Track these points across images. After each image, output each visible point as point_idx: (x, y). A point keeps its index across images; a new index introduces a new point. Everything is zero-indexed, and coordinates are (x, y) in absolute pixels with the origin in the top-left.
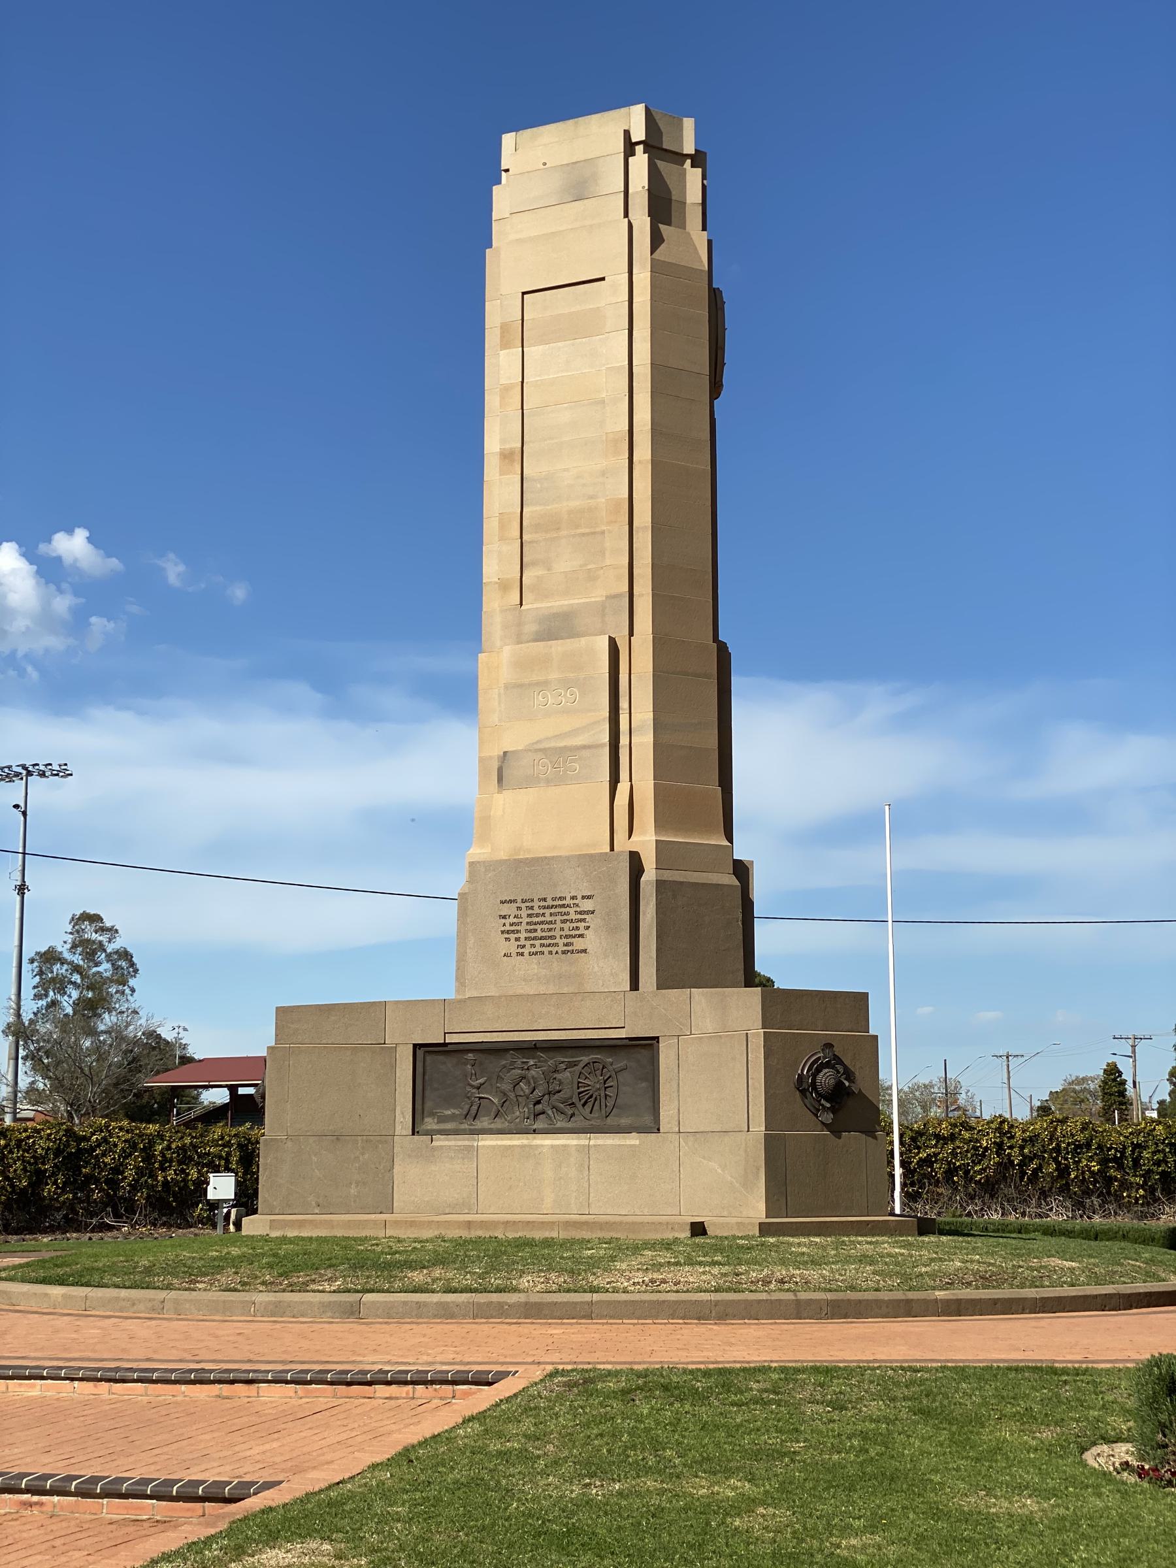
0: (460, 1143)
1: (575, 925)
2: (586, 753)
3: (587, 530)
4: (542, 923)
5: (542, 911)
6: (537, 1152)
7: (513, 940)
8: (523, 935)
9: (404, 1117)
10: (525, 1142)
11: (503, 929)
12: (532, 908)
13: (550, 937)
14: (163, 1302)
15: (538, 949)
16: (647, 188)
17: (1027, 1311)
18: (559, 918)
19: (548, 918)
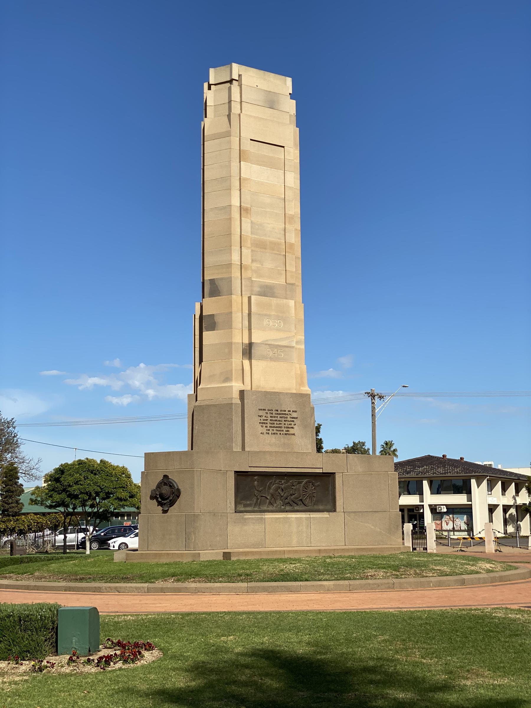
0: (257, 516)
1: (290, 423)
2: (286, 349)
3: (277, 253)
4: (276, 420)
5: (276, 416)
6: (290, 521)
7: (264, 427)
8: (269, 425)
9: (231, 505)
10: (285, 516)
11: (260, 421)
12: (272, 414)
13: (280, 427)
14: (394, 584)
15: (275, 432)
16: (295, 115)
17: (68, 590)
18: (283, 419)
19: (279, 419)
